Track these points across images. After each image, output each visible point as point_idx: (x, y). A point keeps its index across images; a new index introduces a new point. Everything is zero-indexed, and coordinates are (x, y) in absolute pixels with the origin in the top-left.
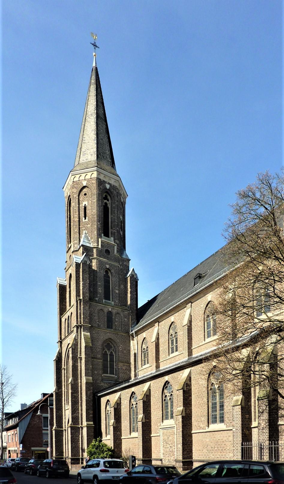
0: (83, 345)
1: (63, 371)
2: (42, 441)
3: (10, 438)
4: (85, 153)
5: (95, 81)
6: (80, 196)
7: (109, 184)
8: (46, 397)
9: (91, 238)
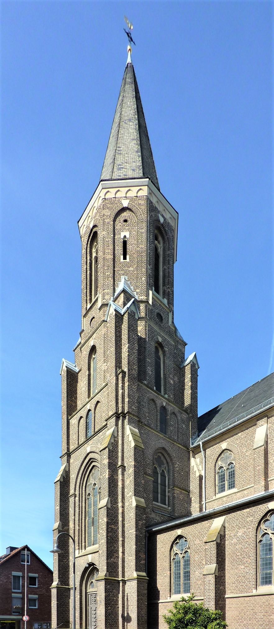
2: (12, 607)
4: (122, 166)
6: (117, 222)
8: (14, 552)
9: (134, 287)
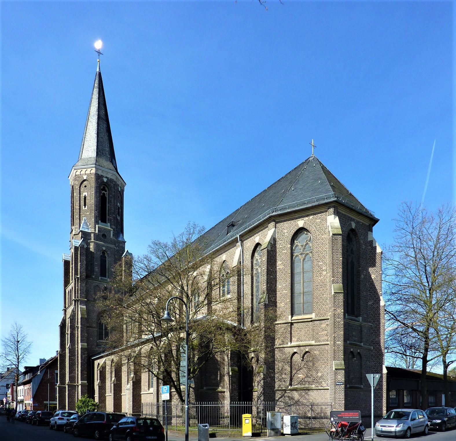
0: (80, 316)
1: (67, 335)
3: (27, 391)
5: (98, 85)
6: (81, 188)
7: (106, 177)
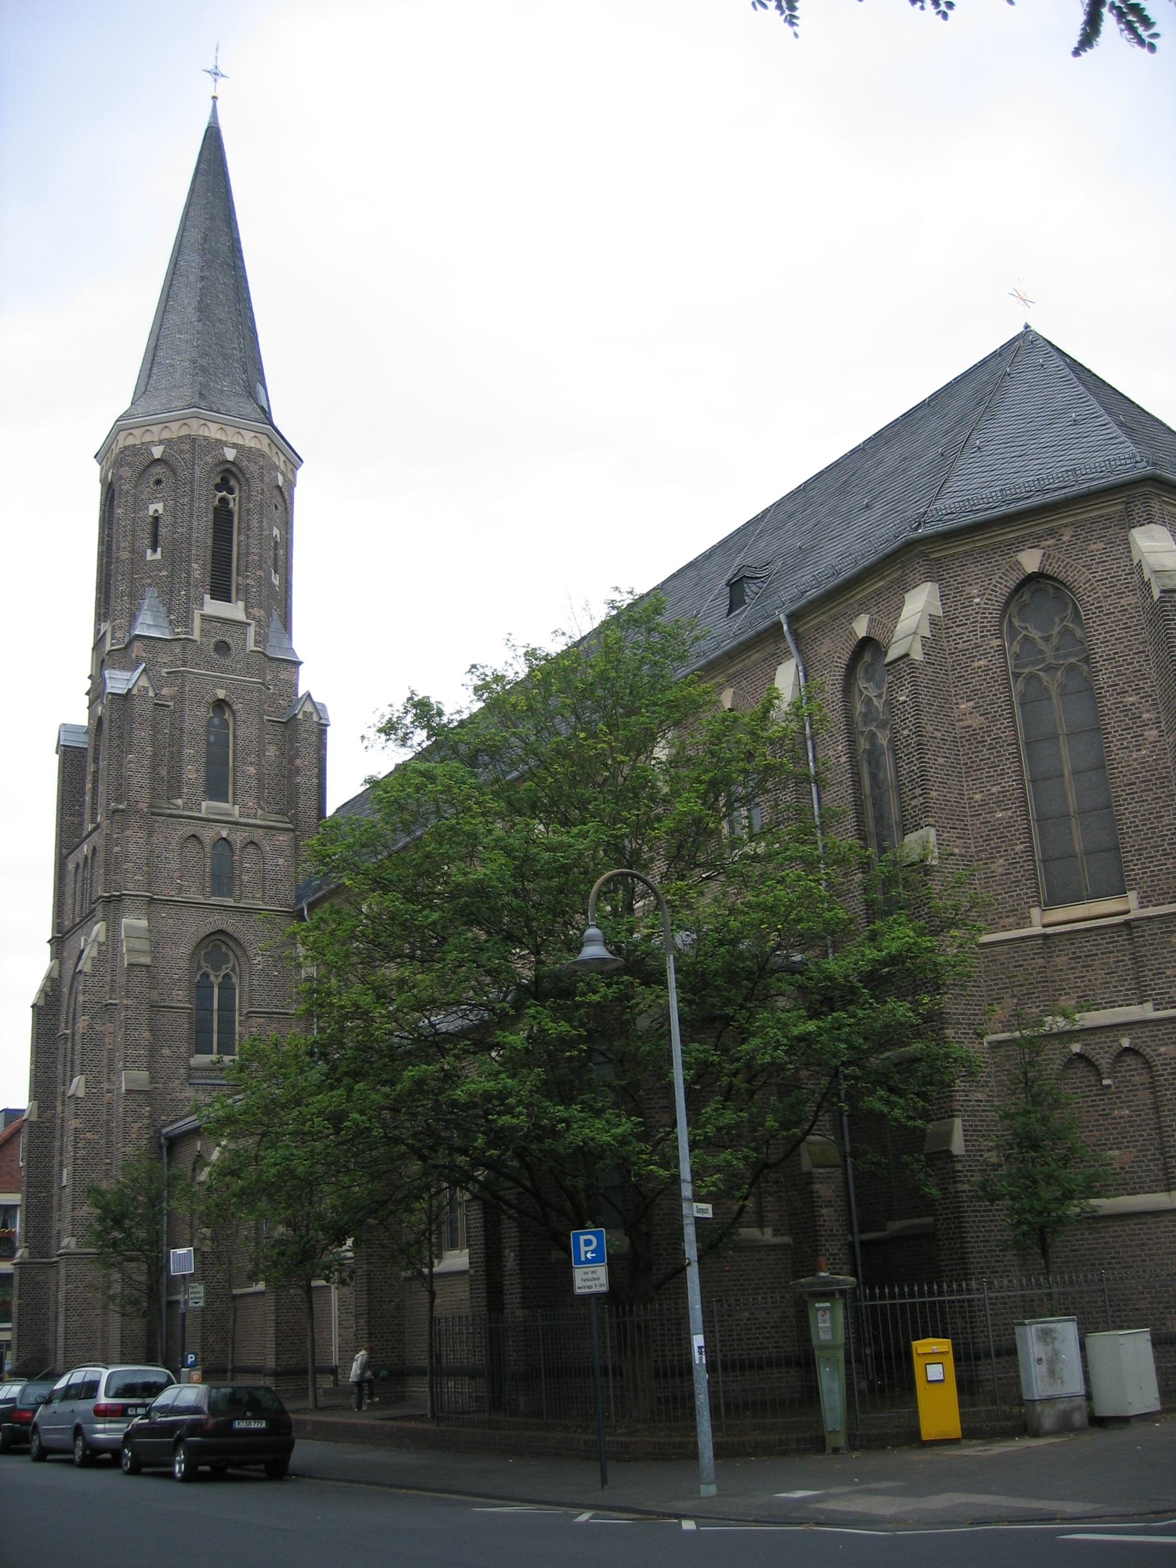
7: (234, 446)
